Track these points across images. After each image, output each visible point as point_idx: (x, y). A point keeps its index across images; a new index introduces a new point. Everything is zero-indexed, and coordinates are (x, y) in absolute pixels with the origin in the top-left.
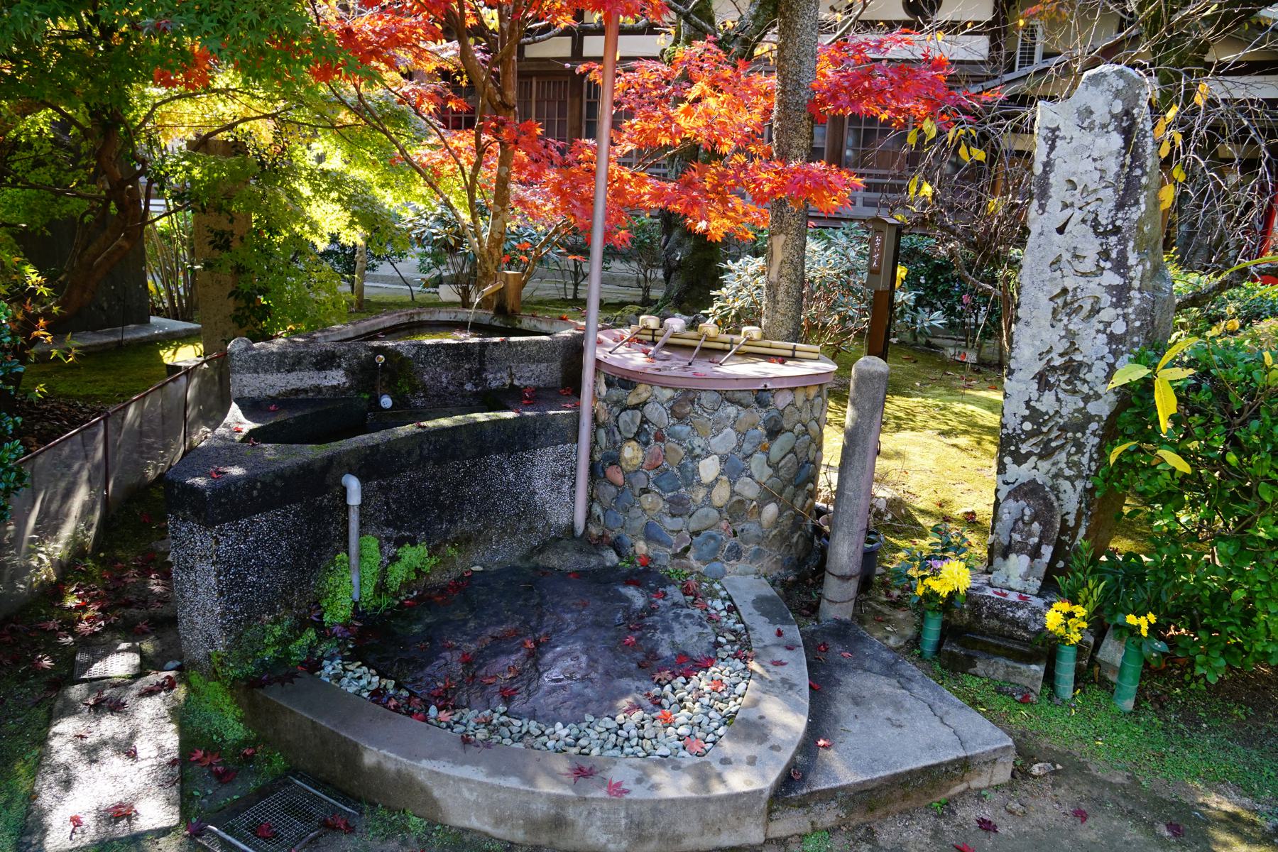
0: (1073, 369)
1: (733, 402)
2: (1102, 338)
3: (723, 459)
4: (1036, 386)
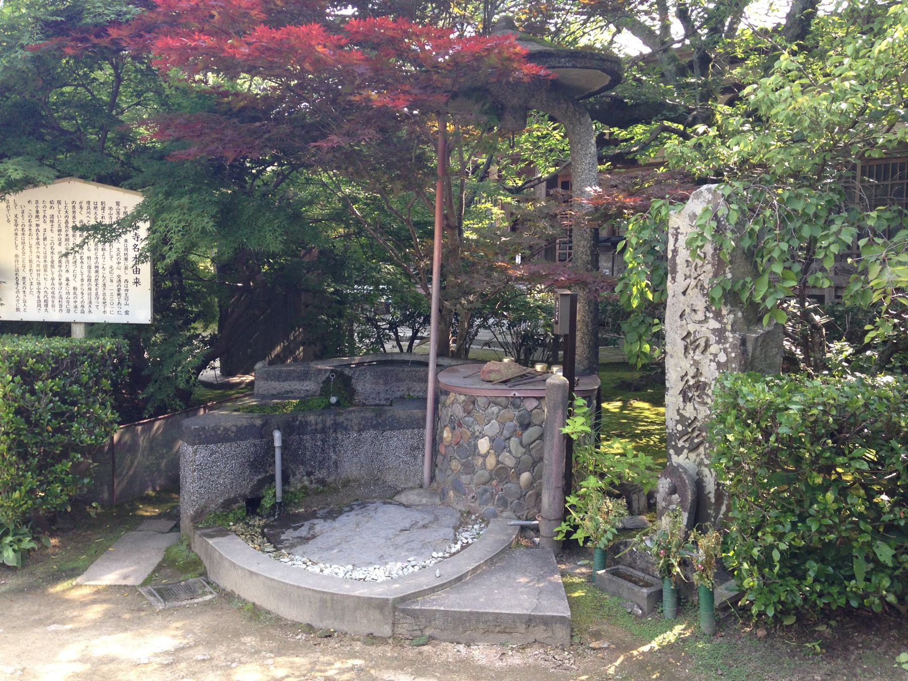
0: (700, 387)
1: (496, 404)
2: (714, 365)
3: (492, 440)
4: (682, 399)
